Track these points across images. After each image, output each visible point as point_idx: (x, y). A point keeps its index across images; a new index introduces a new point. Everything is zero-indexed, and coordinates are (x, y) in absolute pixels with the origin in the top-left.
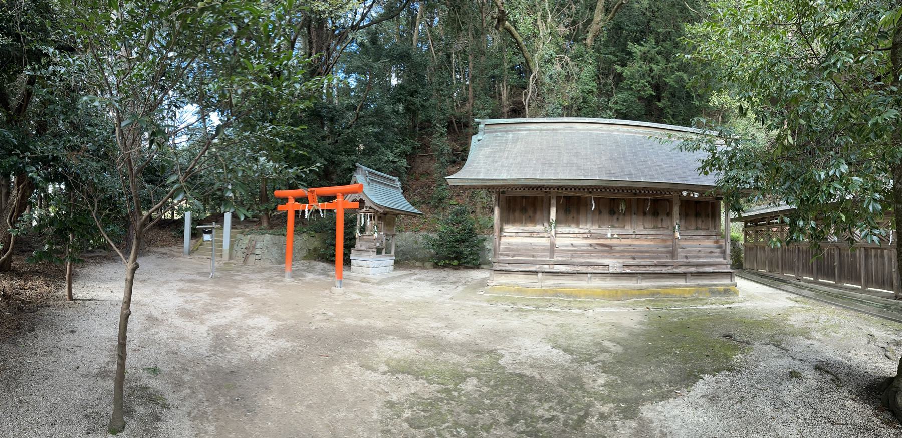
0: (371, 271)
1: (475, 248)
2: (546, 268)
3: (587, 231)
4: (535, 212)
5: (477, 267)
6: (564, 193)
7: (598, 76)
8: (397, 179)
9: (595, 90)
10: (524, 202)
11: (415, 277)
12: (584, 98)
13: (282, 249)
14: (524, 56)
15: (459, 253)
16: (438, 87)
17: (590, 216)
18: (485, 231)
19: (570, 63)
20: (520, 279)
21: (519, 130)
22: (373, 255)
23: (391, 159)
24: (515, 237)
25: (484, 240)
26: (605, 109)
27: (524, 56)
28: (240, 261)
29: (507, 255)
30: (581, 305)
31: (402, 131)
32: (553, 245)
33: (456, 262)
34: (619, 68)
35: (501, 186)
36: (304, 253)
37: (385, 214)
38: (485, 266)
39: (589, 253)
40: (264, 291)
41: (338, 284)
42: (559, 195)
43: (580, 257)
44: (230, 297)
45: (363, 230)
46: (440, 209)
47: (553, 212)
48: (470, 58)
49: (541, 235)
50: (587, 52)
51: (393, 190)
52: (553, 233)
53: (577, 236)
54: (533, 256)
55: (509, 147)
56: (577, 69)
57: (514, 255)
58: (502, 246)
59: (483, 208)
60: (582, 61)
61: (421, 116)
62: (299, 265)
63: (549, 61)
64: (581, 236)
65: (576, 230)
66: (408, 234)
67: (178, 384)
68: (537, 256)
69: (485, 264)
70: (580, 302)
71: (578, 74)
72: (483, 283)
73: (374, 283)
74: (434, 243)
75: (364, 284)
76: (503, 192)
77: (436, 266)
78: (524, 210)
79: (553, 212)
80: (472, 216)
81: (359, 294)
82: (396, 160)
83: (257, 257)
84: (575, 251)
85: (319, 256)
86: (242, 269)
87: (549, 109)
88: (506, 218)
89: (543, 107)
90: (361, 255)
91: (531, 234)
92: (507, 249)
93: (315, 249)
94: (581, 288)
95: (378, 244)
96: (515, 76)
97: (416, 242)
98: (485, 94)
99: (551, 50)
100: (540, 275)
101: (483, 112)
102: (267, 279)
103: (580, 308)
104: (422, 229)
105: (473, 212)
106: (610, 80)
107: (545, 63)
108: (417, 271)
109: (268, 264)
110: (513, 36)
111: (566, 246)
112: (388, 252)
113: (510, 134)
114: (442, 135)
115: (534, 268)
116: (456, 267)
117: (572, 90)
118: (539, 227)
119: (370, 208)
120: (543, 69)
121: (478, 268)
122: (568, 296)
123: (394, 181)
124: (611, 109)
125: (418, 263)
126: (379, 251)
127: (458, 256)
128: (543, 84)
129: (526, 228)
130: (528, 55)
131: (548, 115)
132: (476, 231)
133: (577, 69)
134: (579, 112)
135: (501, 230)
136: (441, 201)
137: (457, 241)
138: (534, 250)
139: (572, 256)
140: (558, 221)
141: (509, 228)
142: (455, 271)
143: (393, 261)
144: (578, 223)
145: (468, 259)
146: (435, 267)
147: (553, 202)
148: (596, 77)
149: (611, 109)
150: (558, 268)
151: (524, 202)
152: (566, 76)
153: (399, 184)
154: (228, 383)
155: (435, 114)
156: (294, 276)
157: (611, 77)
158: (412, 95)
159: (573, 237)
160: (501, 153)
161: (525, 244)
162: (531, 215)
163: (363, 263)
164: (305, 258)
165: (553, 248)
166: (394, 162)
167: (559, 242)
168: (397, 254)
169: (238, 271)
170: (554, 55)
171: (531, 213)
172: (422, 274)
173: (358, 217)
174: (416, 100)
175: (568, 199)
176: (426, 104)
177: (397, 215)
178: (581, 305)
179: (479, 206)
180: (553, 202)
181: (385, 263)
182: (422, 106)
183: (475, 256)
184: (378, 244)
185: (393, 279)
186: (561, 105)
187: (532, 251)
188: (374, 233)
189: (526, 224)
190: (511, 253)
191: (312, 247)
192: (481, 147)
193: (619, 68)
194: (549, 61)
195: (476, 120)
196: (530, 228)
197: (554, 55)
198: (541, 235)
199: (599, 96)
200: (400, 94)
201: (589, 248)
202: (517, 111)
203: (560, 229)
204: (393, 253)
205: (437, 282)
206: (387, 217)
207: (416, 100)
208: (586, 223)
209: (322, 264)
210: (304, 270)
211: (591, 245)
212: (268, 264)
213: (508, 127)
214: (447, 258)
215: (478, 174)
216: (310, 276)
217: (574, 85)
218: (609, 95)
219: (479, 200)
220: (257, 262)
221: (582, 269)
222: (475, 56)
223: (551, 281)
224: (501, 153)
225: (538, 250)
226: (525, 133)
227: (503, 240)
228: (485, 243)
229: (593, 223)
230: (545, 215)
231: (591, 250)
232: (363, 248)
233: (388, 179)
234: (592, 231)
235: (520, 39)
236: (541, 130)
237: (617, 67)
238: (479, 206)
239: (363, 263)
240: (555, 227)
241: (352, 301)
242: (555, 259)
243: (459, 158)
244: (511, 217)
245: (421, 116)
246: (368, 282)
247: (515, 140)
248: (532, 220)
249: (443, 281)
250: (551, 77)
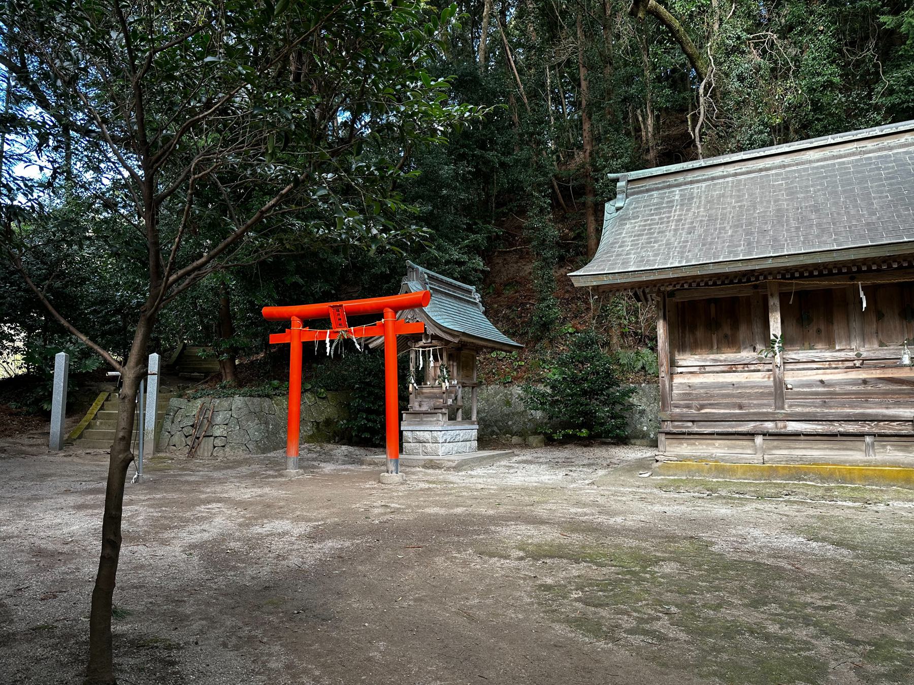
0: (442, 449)
1: (618, 407)
2: (769, 426)
3: (852, 355)
4: (735, 326)
5: (623, 441)
6: (796, 285)
7: (840, 51)
8: (473, 288)
9: (837, 80)
10: (714, 307)
11: (516, 458)
12: (814, 103)
13: (267, 423)
14: (684, 51)
15: (589, 418)
16: (531, 129)
17: (856, 325)
18: (631, 376)
19: (778, 43)
20: (718, 450)
21: (691, 182)
22: (441, 421)
23: (456, 256)
24: (699, 373)
25: (632, 391)
26: (863, 113)
27: (684, 51)
28: (181, 454)
29: (688, 407)
30: (856, 494)
31: (467, 209)
32: (780, 385)
33: (584, 432)
34: (887, 20)
35: (669, 281)
36: (308, 429)
37: (462, 346)
38: (638, 442)
39: (864, 397)
40: (259, 491)
41: (392, 467)
42: (785, 289)
43: (843, 406)
44: (194, 505)
45: (421, 378)
46: (545, 342)
47: (775, 327)
48: (583, 72)
49: (752, 367)
50: (812, 13)
51: (470, 308)
52: (778, 360)
53: (831, 365)
54: (741, 407)
55: (675, 213)
56: (793, 51)
57: (703, 407)
58: (675, 391)
59: (623, 335)
60: (801, 33)
61: (502, 180)
62: (310, 450)
63: (736, 50)
64: (840, 365)
65: (828, 355)
66: (492, 389)
67: (178, 620)
68: (749, 406)
69: (637, 437)
70: (853, 489)
71: (796, 59)
72: (642, 465)
73: (448, 469)
74: (541, 401)
75: (431, 471)
76: (672, 294)
77: (550, 442)
78: (713, 325)
79: (775, 327)
80: (604, 351)
81: (428, 482)
82: (465, 258)
83: (218, 442)
84: (829, 394)
85: (335, 434)
86: (189, 465)
87: (741, 137)
88: (683, 340)
89: (730, 135)
90: (421, 423)
91: (732, 368)
92: (686, 396)
93: (328, 422)
94: (853, 463)
95: (450, 402)
96: (667, 91)
97: (508, 403)
98: (616, 130)
99: (737, 29)
100: (759, 440)
101: (614, 163)
102: (253, 475)
103: (854, 500)
104: (516, 378)
105: (606, 344)
106: (869, 52)
107: (728, 55)
108: (516, 451)
109: (241, 454)
110: (663, 21)
111: (809, 385)
112: (467, 417)
113: (677, 190)
114: (542, 210)
115: (748, 427)
116: (587, 442)
117: (789, 93)
118: (746, 355)
119: (435, 337)
120: (725, 67)
121: (626, 444)
122: (823, 479)
123: (470, 292)
124: (877, 108)
125: (515, 439)
126: (452, 418)
127: (589, 420)
128: (726, 94)
129: (722, 357)
130: (692, 49)
131: (740, 149)
132: (616, 375)
133: (793, 51)
134: (805, 130)
135: (673, 364)
136: (545, 326)
137: (585, 393)
138: (741, 396)
139: (824, 404)
140: (787, 341)
141: (688, 360)
142: (585, 449)
143: (474, 433)
144: (830, 344)
145: (608, 427)
146: (546, 445)
147: (774, 302)
148: (835, 55)
149: (877, 108)
150: (793, 427)
151: (714, 307)
152: (773, 70)
153: (477, 297)
154: (266, 605)
155: (526, 177)
156: (302, 464)
157: (872, 44)
158: (483, 147)
159: (818, 368)
160: (657, 227)
161: (723, 386)
162: (729, 333)
163: (427, 435)
164: (311, 439)
165: (780, 390)
166: (460, 263)
167: (791, 378)
168: (480, 421)
169: (183, 469)
170: (744, 36)
171: (727, 330)
172: (527, 455)
173: (413, 356)
174: (490, 155)
175: (802, 295)
176: (507, 160)
177: (478, 349)
178: (856, 494)
179: (615, 332)
180: (774, 302)
181: (463, 435)
182: (503, 165)
183: (619, 421)
184: (450, 402)
185: (480, 461)
186: (766, 125)
187: (737, 396)
188: (441, 380)
189: (719, 351)
190: (695, 403)
191: (321, 419)
192: (623, 220)
193: (887, 20)
194: (736, 50)
195: (611, 176)
196: (729, 356)
197: (744, 36)
198: (752, 367)
199: (845, 90)
200: (463, 146)
201: (862, 388)
202: (677, 150)
203: (792, 355)
204: (474, 418)
205: (555, 465)
206: (462, 352)
207: (490, 155)
208: (849, 339)
209: (344, 448)
210: (314, 460)
211: (865, 382)
212: (241, 454)
213: (671, 180)
214: (565, 425)
215: (626, 263)
216: (328, 468)
217: (791, 82)
218: (869, 81)
219: (615, 322)
220: (219, 453)
221: (851, 428)
222: (591, 67)
223: (782, 453)
224: (657, 227)
225: (749, 396)
226: (704, 185)
227: (677, 380)
228: (634, 400)
229: (864, 338)
230: (757, 329)
231: (864, 392)
232: (425, 408)
233: (459, 288)
234: (865, 355)
235: (677, 24)
236: (736, 175)
237: (883, 19)
238: (615, 332)
239: (427, 435)
240: (782, 349)
241: (421, 490)
242: (788, 410)
243: (581, 248)
244: (689, 338)
245: (502, 180)
246: (439, 467)
247: (687, 200)
248: (732, 342)
249: (568, 463)
250: (741, 78)
